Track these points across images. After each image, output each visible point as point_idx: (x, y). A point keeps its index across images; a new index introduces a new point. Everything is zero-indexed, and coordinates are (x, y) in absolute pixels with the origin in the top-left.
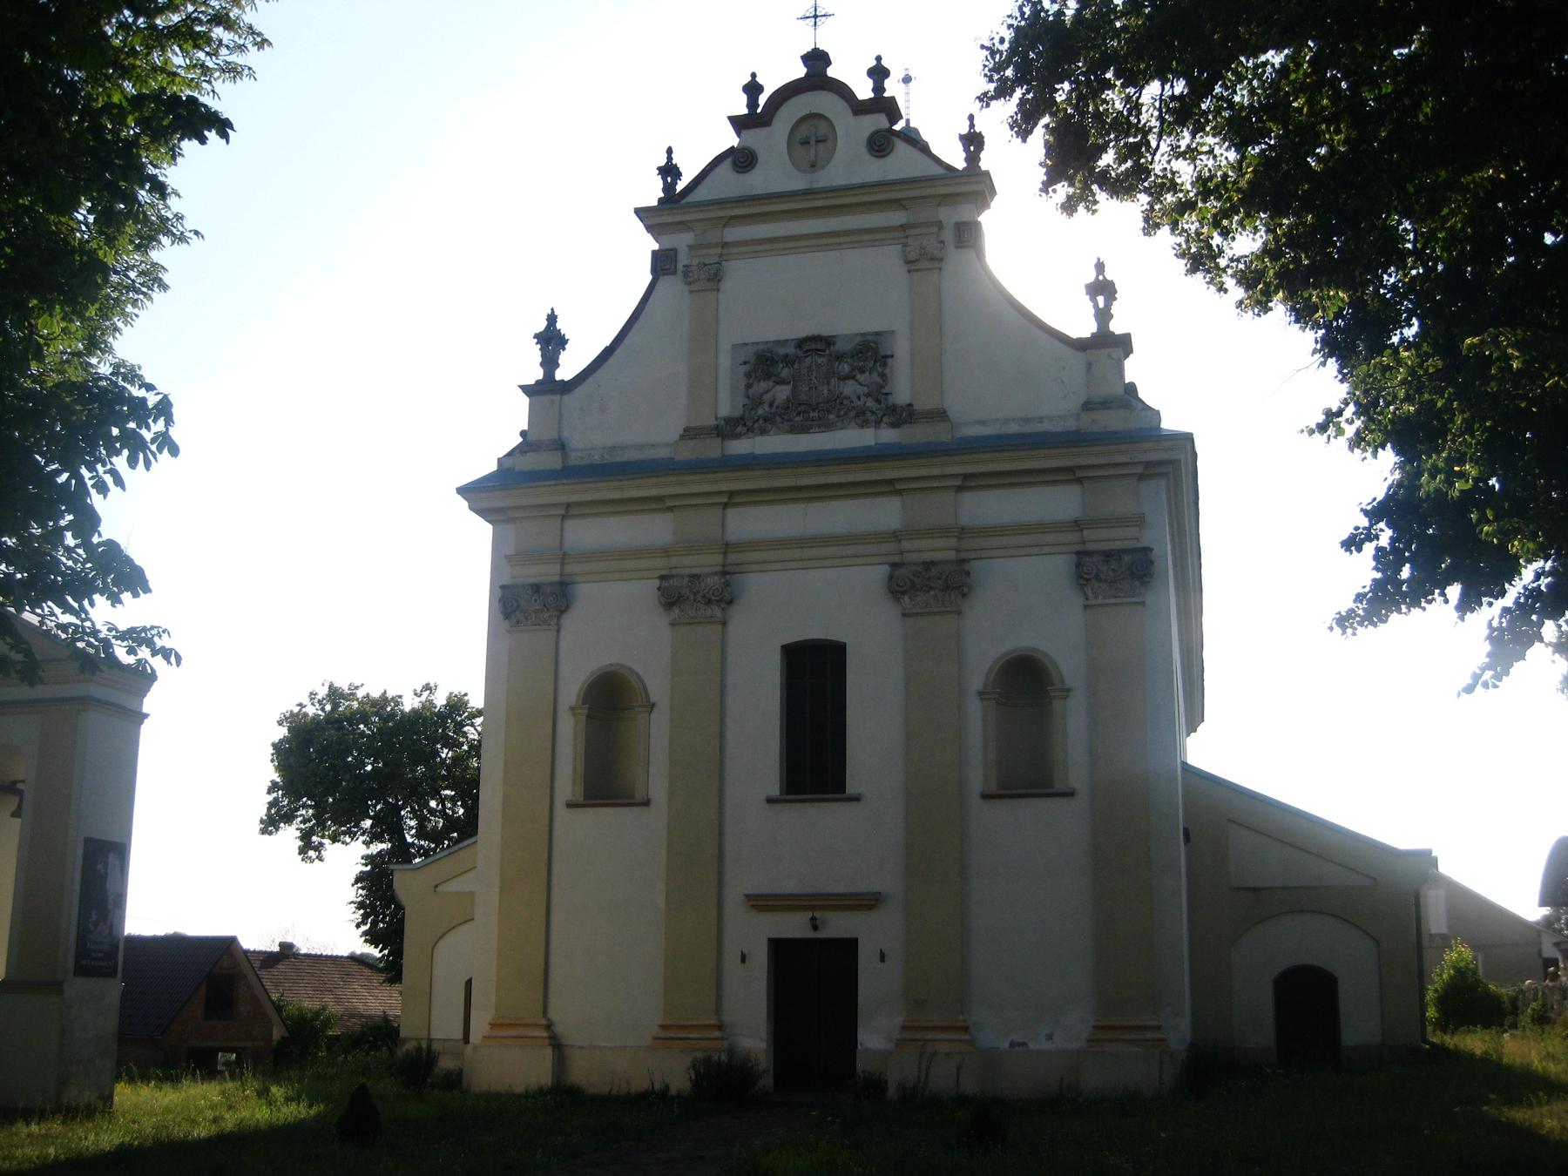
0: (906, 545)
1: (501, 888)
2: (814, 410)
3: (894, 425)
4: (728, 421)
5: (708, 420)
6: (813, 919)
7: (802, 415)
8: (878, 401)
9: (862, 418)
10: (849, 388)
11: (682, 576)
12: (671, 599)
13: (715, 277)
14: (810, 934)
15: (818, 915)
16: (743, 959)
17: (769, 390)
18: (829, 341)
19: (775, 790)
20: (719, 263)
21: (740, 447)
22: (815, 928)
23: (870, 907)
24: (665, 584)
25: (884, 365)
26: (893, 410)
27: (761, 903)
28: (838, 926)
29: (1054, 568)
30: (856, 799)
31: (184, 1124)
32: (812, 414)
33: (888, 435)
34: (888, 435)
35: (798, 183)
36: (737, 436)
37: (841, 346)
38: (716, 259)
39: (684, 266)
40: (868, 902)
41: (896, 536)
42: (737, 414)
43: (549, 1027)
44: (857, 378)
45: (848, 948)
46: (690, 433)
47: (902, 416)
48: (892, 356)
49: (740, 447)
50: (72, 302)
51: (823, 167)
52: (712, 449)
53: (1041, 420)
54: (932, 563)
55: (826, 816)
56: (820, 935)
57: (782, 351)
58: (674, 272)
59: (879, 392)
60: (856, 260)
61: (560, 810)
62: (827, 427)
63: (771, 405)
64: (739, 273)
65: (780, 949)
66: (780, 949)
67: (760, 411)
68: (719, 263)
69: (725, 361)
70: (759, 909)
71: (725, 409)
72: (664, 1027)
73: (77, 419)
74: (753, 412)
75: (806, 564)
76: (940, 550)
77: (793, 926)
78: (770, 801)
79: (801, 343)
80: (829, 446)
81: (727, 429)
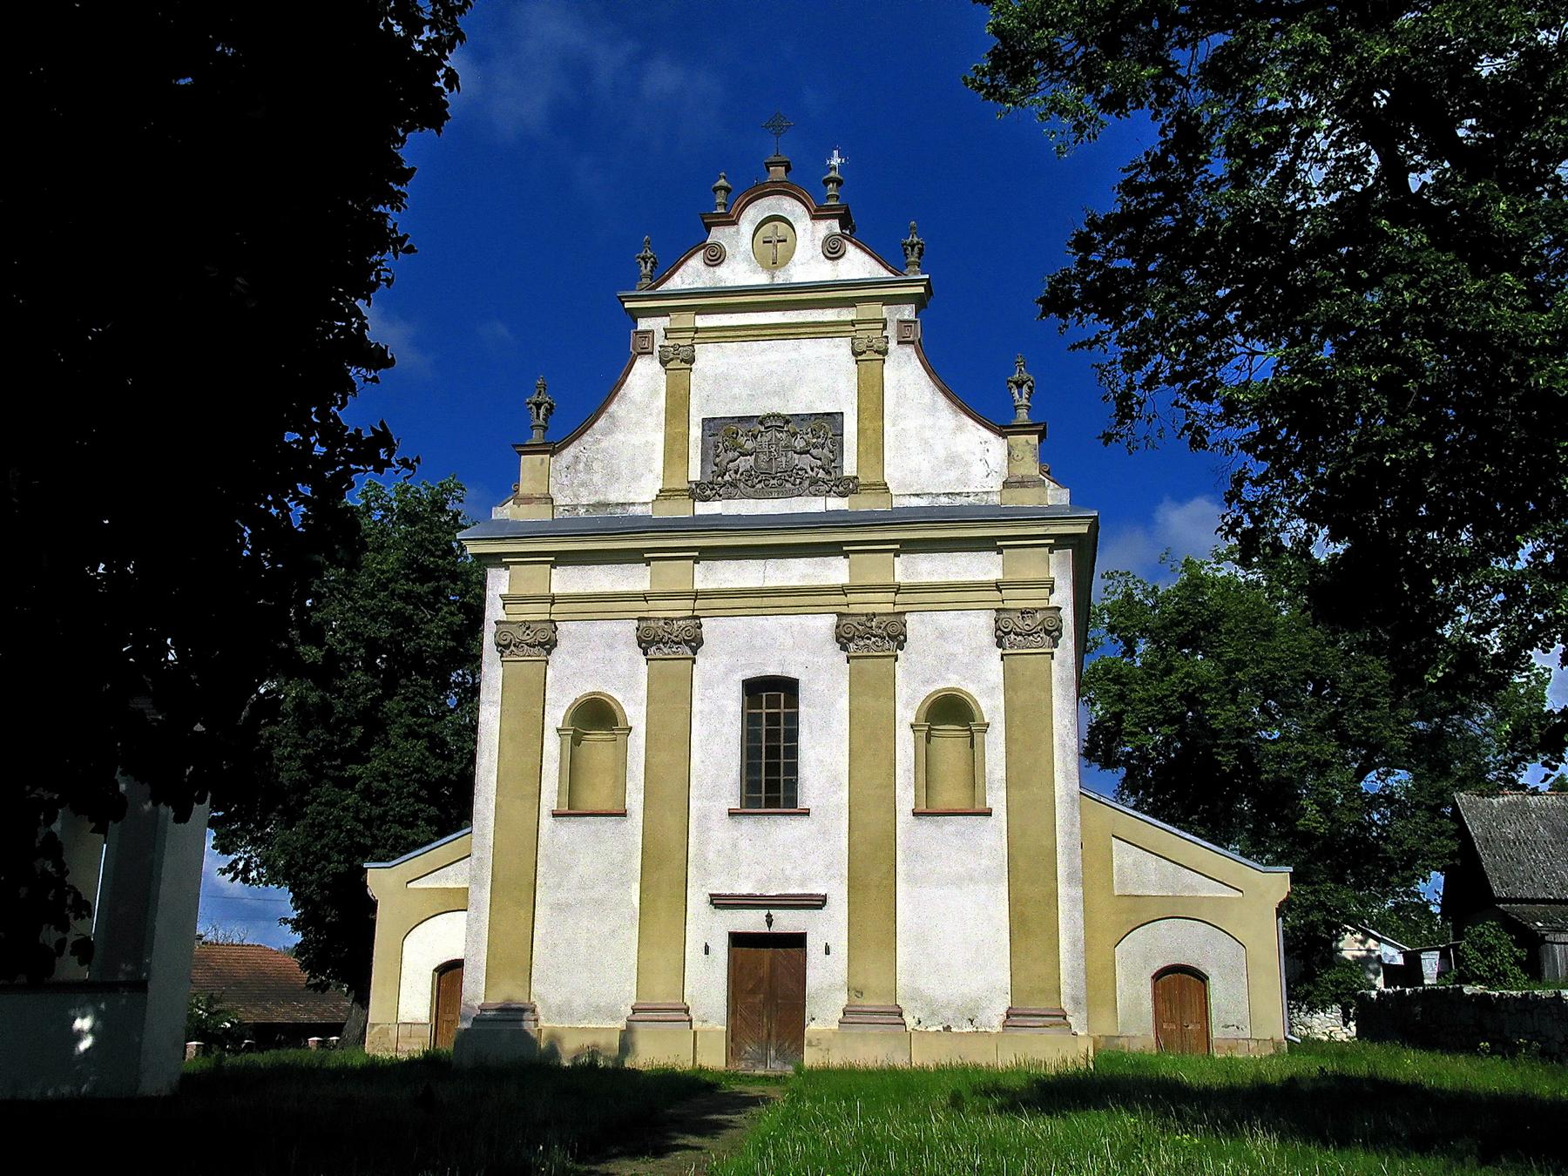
0: (852, 598)
2: (774, 479)
6: (769, 916)
8: (828, 473)
9: (816, 487)
11: (659, 619)
12: (646, 642)
14: (765, 930)
15: (772, 912)
17: (736, 460)
19: (736, 805)
20: (692, 345)
21: (702, 509)
22: (770, 923)
23: (820, 907)
24: (644, 624)
26: (841, 481)
27: (720, 902)
28: (786, 922)
30: (806, 813)
31: (913, 686)
32: (772, 482)
33: (836, 504)
34: (836, 504)
35: (762, 279)
38: (689, 342)
39: (660, 346)
40: (816, 903)
41: (998, 586)
44: (1540, 790)
45: (797, 941)
49: (702, 509)
52: (681, 509)
54: (874, 614)
55: (783, 830)
56: (774, 930)
60: (810, 349)
61: (546, 822)
63: (736, 472)
64: (709, 358)
65: (738, 940)
66: (738, 940)
67: (727, 477)
68: (692, 345)
70: (717, 906)
71: (695, 474)
74: (720, 478)
75: (765, 611)
76: (881, 604)
77: (752, 922)
78: (732, 814)
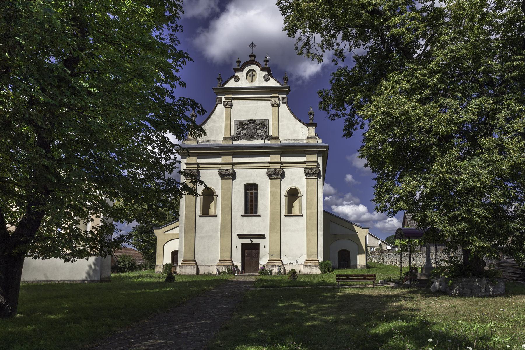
1: (270, 230)
3: (268, 140)
4: (233, 136)
5: (229, 136)
7: (249, 136)
9: (261, 137)
10: (259, 131)
13: (231, 106)
16: (236, 247)
18: (254, 121)
19: (243, 214)
25: (266, 127)
27: (240, 236)
28: (255, 241)
29: (301, 172)
30: (260, 216)
33: (267, 142)
34: (267, 142)
36: (235, 140)
37: (257, 122)
40: (263, 237)
42: (235, 135)
43: (195, 261)
46: (225, 139)
47: (270, 138)
48: (268, 125)
50: (458, 265)
51: (254, 81)
52: (229, 143)
53: (298, 140)
57: (245, 122)
58: (221, 103)
59: (265, 132)
61: (197, 217)
62: (255, 139)
65: (243, 245)
66: (243, 245)
69: (233, 123)
71: (232, 134)
72: (220, 261)
73: (490, 267)
77: (247, 241)
78: (242, 216)
79: (249, 121)
80: (257, 143)
81: (233, 138)
